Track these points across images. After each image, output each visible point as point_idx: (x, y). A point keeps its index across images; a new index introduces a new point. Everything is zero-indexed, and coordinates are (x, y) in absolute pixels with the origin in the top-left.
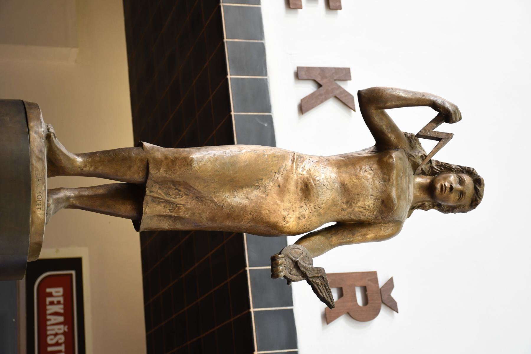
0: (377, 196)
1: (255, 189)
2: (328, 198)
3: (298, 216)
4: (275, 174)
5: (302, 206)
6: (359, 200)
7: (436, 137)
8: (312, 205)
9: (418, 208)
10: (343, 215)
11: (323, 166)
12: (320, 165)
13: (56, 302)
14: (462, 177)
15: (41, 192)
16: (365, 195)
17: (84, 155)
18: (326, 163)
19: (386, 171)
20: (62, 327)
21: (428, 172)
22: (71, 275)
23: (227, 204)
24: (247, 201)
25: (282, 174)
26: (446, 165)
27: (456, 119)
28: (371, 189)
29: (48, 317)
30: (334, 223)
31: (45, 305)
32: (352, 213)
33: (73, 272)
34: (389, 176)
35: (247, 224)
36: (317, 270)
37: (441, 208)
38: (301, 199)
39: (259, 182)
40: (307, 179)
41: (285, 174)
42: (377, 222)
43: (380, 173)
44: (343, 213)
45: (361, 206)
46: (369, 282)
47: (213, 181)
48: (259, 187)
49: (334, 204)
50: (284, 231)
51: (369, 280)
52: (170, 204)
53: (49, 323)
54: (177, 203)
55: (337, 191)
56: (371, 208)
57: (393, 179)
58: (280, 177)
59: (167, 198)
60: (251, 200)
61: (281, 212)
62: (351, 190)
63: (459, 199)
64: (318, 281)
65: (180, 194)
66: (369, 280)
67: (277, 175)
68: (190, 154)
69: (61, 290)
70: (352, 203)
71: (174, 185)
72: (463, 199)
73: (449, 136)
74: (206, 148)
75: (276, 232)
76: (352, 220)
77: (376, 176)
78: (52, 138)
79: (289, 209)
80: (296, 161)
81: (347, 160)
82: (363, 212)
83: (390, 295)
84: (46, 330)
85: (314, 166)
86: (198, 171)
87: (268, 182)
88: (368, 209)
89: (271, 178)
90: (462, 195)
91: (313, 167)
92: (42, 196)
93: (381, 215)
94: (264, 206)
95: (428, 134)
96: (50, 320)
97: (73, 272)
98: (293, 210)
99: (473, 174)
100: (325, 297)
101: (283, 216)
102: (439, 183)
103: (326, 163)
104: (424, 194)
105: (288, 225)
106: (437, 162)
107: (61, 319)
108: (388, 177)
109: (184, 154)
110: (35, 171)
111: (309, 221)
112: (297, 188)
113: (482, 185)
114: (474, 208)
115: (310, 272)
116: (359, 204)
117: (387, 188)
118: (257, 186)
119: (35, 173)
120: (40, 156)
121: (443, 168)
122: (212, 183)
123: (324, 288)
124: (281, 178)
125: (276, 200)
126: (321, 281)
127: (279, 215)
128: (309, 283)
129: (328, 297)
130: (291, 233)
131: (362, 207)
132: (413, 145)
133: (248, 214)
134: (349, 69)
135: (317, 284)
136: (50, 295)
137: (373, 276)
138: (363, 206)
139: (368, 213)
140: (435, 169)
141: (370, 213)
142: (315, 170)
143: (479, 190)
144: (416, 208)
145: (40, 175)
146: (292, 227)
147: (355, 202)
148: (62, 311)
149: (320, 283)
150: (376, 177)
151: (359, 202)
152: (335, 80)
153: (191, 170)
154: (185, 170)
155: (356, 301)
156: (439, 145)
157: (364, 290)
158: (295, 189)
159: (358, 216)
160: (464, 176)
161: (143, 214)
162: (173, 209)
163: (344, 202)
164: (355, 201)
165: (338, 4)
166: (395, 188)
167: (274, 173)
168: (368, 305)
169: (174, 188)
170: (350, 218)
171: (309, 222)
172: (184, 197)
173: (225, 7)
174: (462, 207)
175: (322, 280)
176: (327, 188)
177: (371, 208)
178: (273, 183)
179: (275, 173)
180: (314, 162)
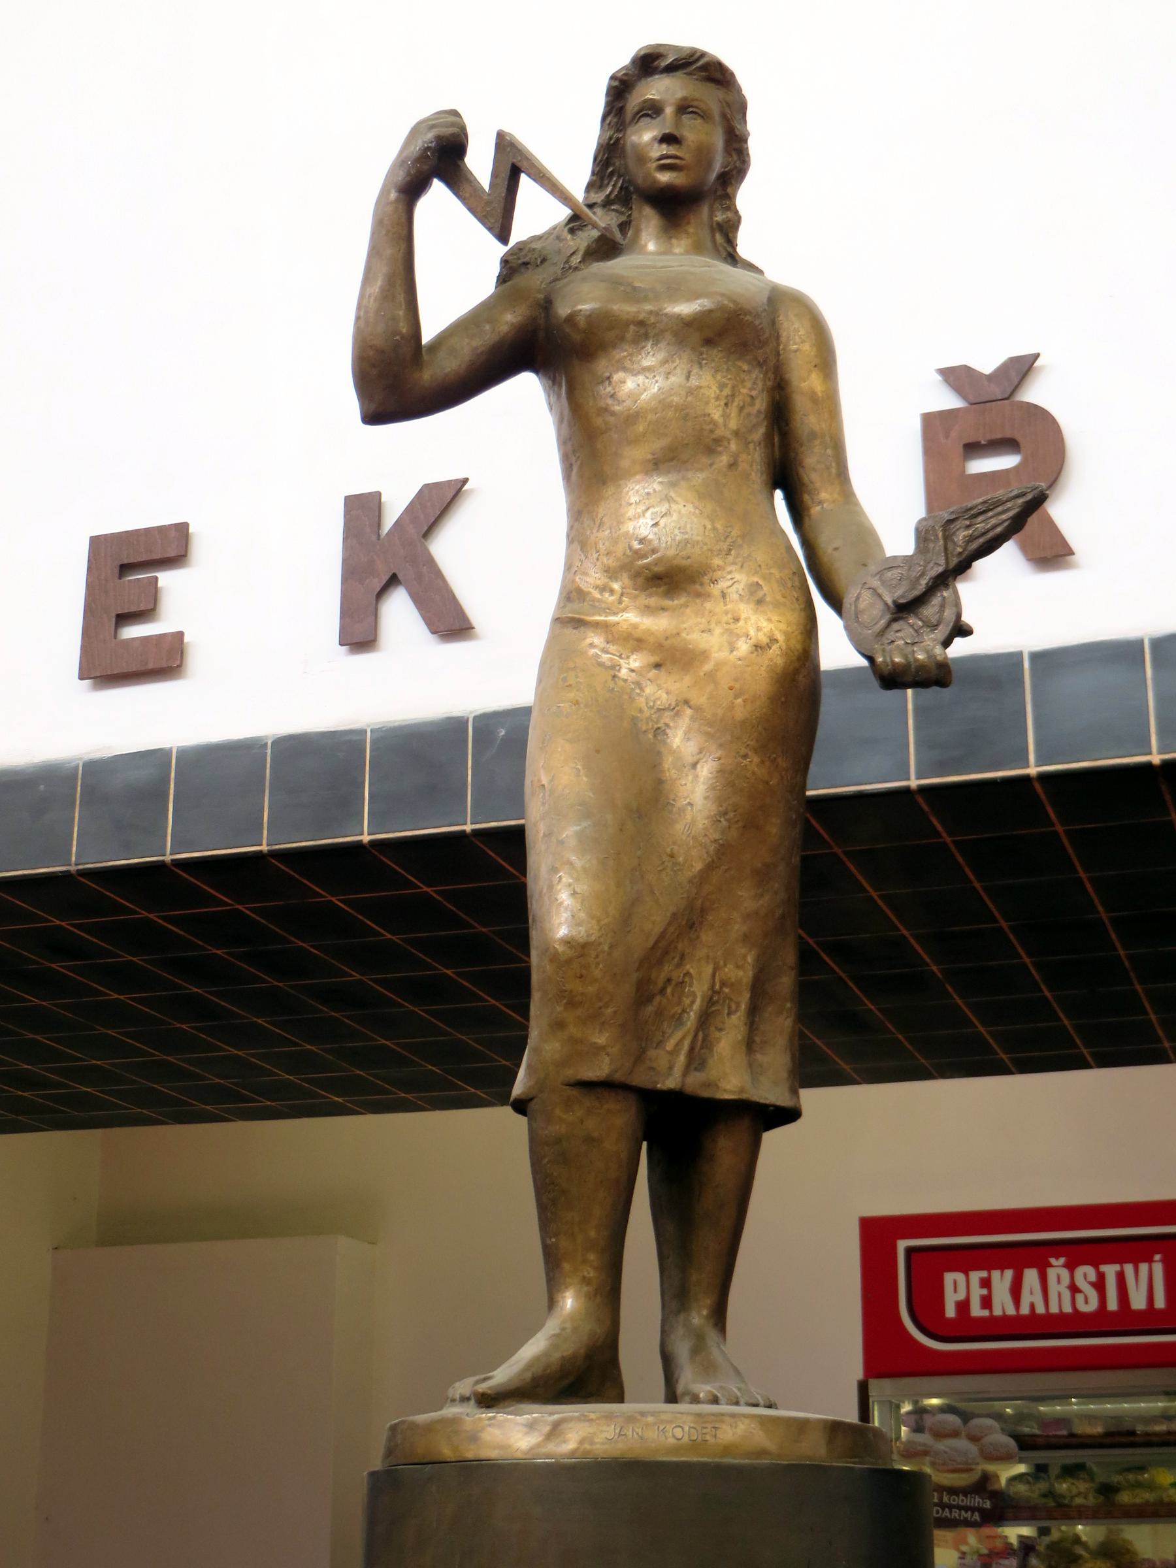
0: (692, 361)
1: (664, 743)
2: (697, 511)
3: (752, 606)
4: (619, 677)
5: (722, 592)
6: (705, 415)
7: (506, 183)
8: (717, 561)
9: (731, 242)
10: (751, 466)
11: (595, 531)
12: (593, 538)
13: (985, 1292)
14: (636, 109)
15: (661, 1428)
16: (687, 397)
17: (552, 1283)
18: (587, 522)
19: (611, 335)
20: (1052, 1273)
21: (622, 213)
22: (910, 1251)
23: (711, 831)
24: (702, 767)
25: (620, 656)
26: (601, 161)
27: (453, 125)
28: (667, 378)
29: (1025, 1310)
30: (779, 495)
31: (992, 1319)
32: (746, 439)
33: (902, 1245)
34: (628, 324)
35: (777, 766)
36: (926, 540)
37: (733, 176)
38: (699, 595)
39: (644, 728)
40: (635, 577)
41: (620, 649)
42: (772, 363)
43: (618, 350)
44: (743, 466)
45: (721, 409)
46: (953, 434)
47: (638, 873)
48: (659, 728)
49: (711, 494)
50: (801, 650)
51: (947, 437)
52: (713, 1012)
53: (1040, 1309)
54: (709, 989)
55: (673, 485)
56: (729, 379)
57: (638, 312)
58: (629, 663)
59: (691, 1019)
60: (701, 755)
61: (740, 659)
62: (669, 439)
63: (704, 116)
64: (961, 536)
65: (681, 980)
66: (947, 437)
67: (624, 673)
68: (547, 950)
69: (949, 1278)
70: (714, 436)
71: (650, 999)
72: (702, 106)
73: (505, 145)
74: (532, 897)
75: (804, 677)
76: (768, 437)
77: (628, 364)
78: (490, 1388)
79: (730, 632)
80: (580, 613)
81: (578, 457)
82: (741, 404)
83: (991, 378)
84: (1062, 1316)
85: (595, 556)
86: (603, 923)
87: (642, 699)
88: (733, 387)
89: (633, 690)
90: (691, 110)
91: (598, 559)
92: (674, 1425)
93: (752, 347)
94: (720, 712)
95: (498, 207)
96: (1032, 1306)
97: (902, 1245)
98: (732, 621)
99: (625, 78)
100: (1010, 514)
101: (752, 653)
102: (654, 178)
103: (587, 522)
104: (688, 223)
105: (779, 636)
106: (590, 187)
107: (1031, 1276)
108: (632, 328)
109: (548, 967)
110: (594, 1447)
111: (768, 572)
112: (663, 609)
113: (662, 50)
114: (732, 75)
115: (931, 565)
116: (717, 415)
117: (666, 331)
118: (655, 736)
119: (598, 1446)
120: (547, 1429)
121: (611, 169)
122: (642, 877)
123: (980, 518)
124: (631, 660)
125: (702, 674)
126: (958, 527)
127: (748, 666)
128: (962, 567)
129: (1009, 505)
130: (808, 627)
131: (726, 404)
132: (536, 259)
133: (746, 765)
134: (347, 499)
135: (971, 539)
136: (963, 1307)
137: (934, 425)
138: (722, 403)
139: (744, 387)
140: (611, 192)
141: (743, 381)
142: (608, 554)
143: (673, 60)
144: (730, 249)
145: (608, 1429)
146: (789, 624)
147: (711, 426)
148: (1009, 1274)
149: (966, 533)
150: (633, 362)
151: (709, 415)
152: (379, 535)
153: (600, 944)
154: (598, 964)
155: (1006, 472)
156: (532, 171)
157: (974, 449)
158: (666, 614)
159: (754, 421)
160: (634, 104)
161: (744, 1096)
162: (727, 1001)
163: (709, 462)
164: (708, 427)
165: (173, 534)
166: (666, 306)
167: (615, 683)
168: (1018, 436)
169: (658, 999)
170: (762, 445)
171: (773, 571)
172: (688, 967)
173: (177, 847)
174: (727, 111)
175: (958, 524)
176: (666, 514)
177: (729, 379)
178: (646, 686)
179: (617, 679)
180: (583, 558)
